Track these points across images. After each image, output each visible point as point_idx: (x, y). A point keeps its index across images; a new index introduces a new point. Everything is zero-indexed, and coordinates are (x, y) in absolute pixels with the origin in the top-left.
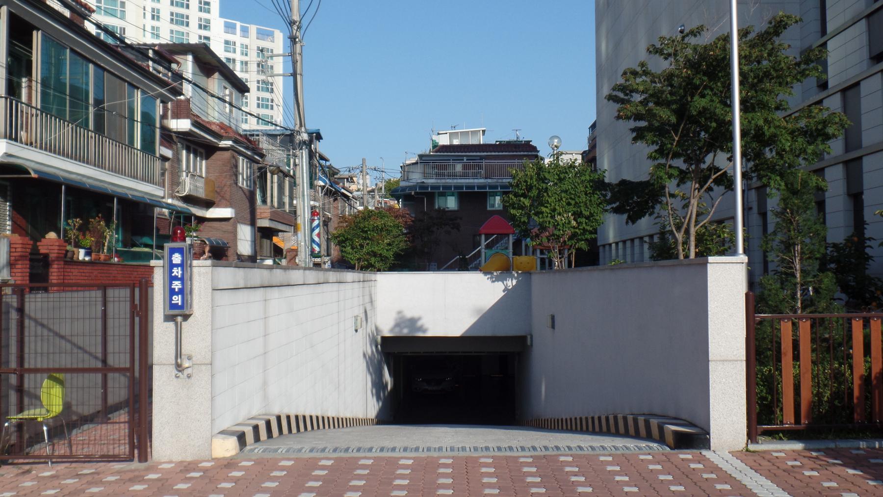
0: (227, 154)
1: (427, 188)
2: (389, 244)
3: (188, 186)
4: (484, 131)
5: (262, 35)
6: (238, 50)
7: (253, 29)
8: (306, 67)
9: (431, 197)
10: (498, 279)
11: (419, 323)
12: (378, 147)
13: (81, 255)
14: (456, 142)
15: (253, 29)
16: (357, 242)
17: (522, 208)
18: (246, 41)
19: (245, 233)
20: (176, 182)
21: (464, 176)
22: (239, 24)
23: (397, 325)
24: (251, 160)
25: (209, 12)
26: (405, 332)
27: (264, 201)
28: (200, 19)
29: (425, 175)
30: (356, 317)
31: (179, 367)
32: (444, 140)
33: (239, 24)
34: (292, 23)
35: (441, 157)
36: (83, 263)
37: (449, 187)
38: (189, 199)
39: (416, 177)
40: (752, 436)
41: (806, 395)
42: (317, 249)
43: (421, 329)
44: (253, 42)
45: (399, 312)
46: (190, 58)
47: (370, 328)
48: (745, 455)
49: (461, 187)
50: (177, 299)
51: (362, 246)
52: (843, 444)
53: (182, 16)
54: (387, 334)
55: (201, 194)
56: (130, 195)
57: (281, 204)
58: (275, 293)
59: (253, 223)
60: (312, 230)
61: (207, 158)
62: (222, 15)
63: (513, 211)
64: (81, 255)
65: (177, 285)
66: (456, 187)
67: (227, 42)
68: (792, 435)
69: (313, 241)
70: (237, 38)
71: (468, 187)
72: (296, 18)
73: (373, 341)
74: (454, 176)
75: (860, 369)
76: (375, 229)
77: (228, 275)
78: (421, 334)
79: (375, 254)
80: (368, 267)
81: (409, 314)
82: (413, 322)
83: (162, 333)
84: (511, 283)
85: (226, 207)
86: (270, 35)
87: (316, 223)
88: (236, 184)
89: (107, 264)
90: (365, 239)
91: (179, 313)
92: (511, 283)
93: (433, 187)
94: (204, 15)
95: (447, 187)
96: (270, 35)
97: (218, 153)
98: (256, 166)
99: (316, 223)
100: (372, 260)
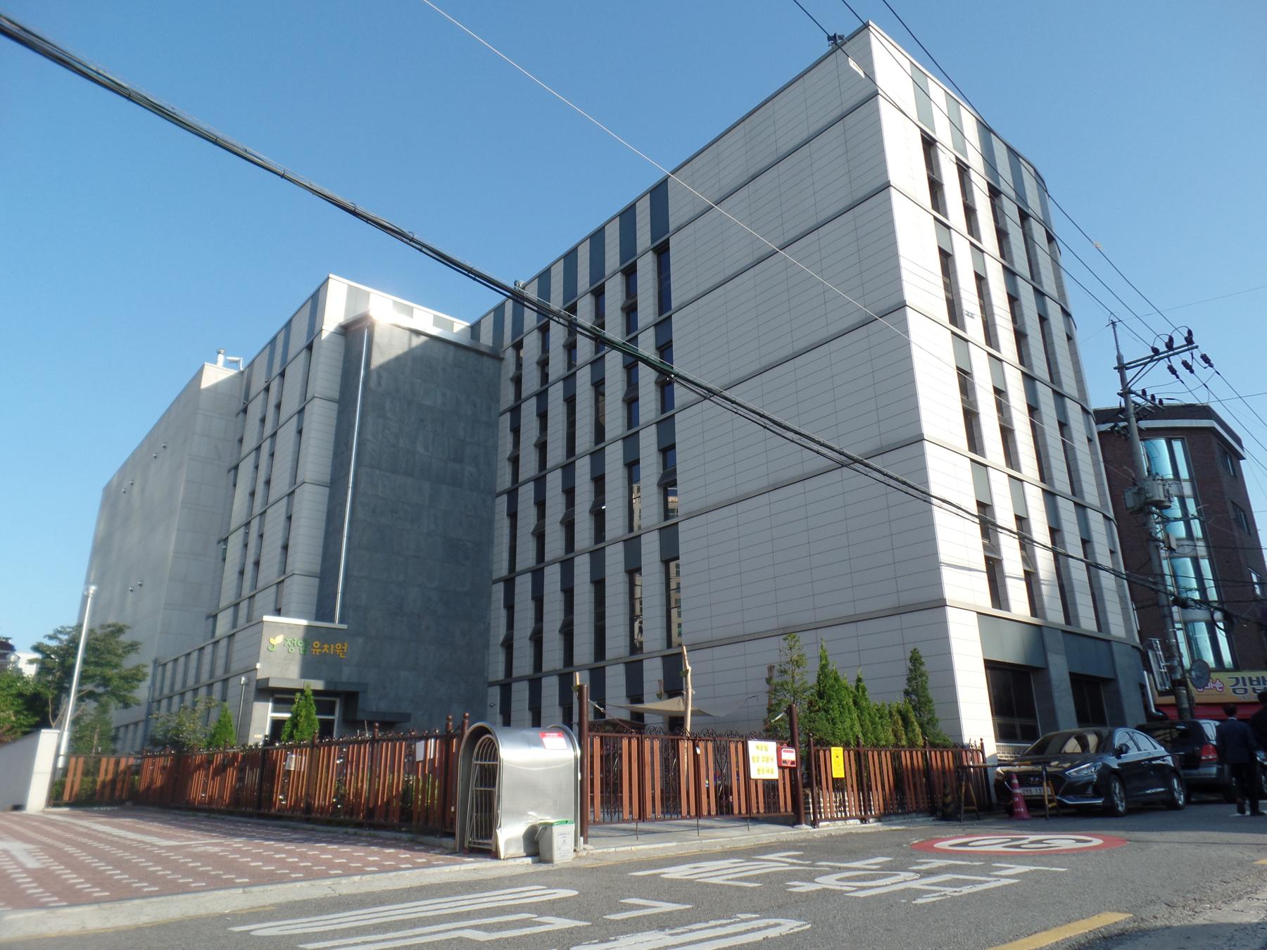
68: (66, 805)
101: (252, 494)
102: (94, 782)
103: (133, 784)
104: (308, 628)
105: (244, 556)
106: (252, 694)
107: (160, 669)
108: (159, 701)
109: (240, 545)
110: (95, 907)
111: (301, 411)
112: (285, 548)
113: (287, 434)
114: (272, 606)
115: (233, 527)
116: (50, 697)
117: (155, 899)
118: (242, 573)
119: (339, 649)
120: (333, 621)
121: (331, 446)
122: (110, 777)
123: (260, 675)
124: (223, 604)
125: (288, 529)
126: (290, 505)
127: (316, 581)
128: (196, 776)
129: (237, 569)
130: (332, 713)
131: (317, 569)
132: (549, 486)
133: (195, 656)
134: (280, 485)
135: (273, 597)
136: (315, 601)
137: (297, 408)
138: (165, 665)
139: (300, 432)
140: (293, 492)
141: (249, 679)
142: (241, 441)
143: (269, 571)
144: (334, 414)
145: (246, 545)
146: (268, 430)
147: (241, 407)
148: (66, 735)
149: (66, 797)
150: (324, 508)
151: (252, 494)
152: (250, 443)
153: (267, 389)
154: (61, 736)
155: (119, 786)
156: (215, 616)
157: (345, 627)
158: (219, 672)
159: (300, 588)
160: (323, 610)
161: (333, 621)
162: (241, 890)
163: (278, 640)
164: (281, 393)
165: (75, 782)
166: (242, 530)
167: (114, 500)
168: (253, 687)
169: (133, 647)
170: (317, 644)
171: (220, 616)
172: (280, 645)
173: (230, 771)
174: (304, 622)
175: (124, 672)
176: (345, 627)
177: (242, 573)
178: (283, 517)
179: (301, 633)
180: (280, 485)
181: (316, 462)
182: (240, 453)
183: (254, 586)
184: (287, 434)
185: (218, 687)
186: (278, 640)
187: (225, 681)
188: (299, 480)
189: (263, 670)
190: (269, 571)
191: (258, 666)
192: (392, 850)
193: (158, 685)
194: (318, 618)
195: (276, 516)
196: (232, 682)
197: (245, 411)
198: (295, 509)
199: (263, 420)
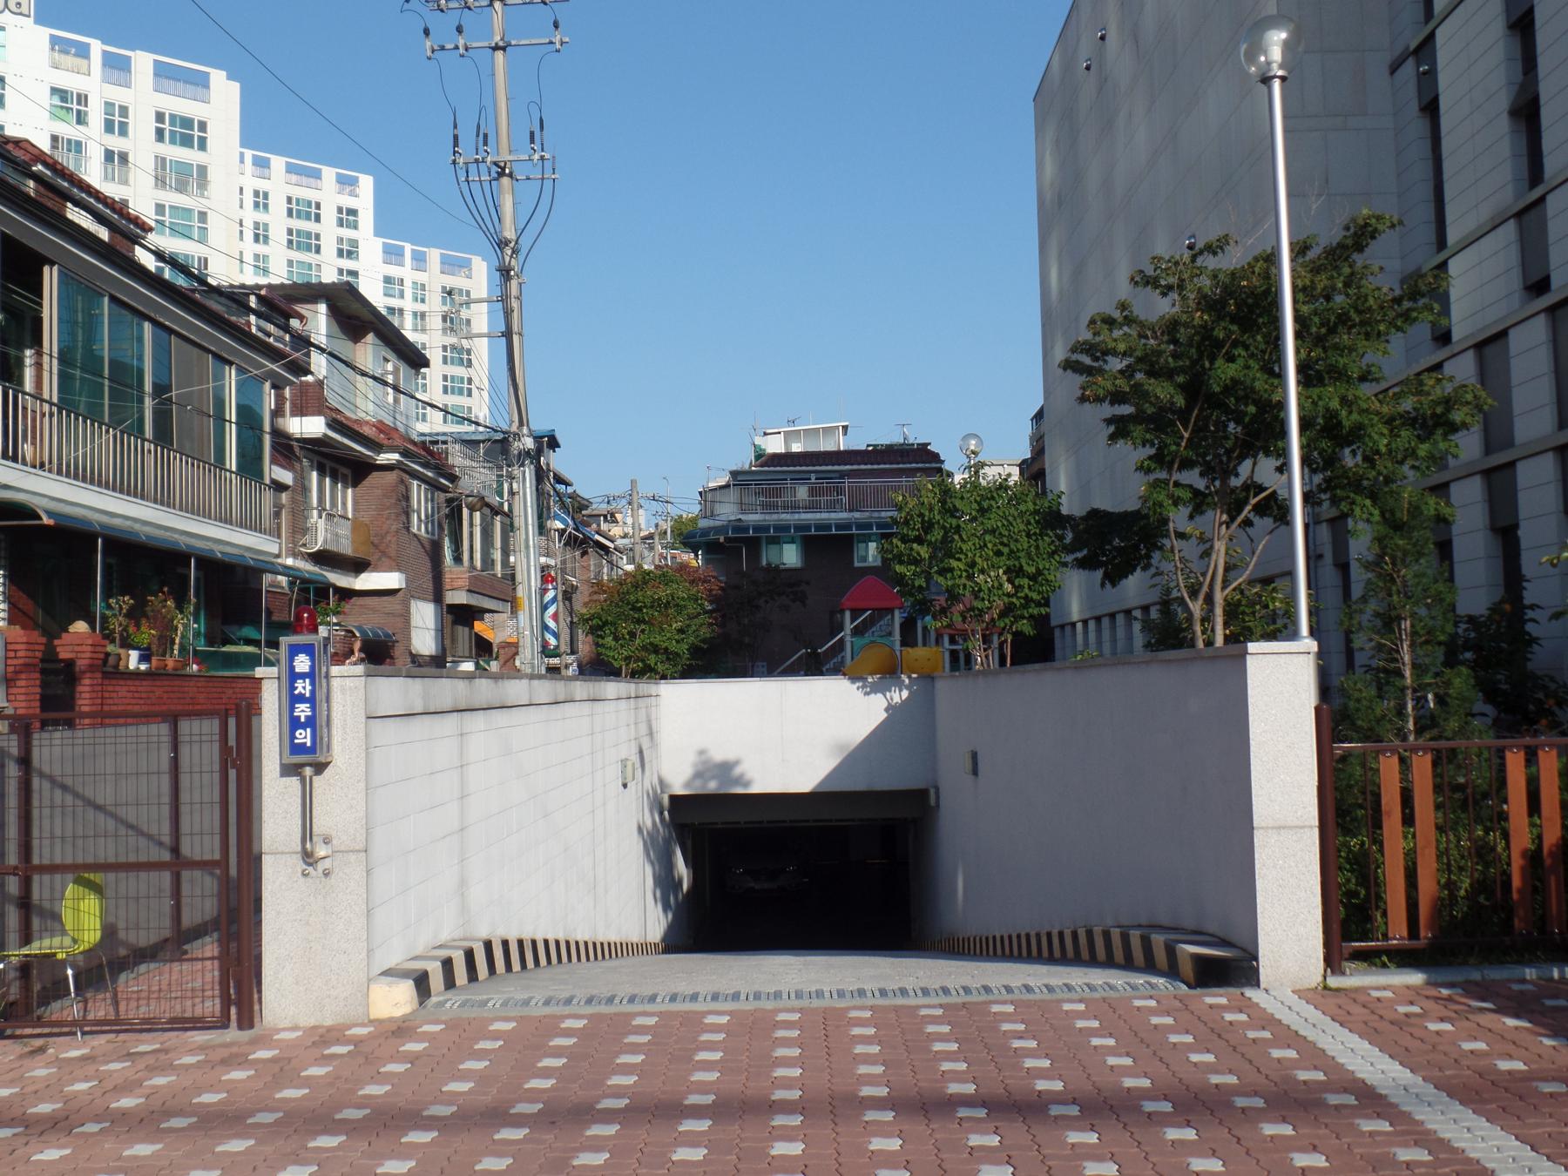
0: (391, 477)
1: (746, 529)
2: (681, 631)
3: (321, 535)
5: (449, 265)
6: (408, 293)
7: (434, 255)
8: (530, 321)
10: (875, 689)
11: (737, 771)
12: (655, 462)
14: (796, 448)
15: (434, 255)
16: (624, 628)
17: (916, 562)
18: (422, 277)
20: (300, 528)
21: (812, 507)
23: (698, 775)
24: (434, 486)
25: (356, 228)
26: (712, 786)
27: (458, 559)
28: (340, 240)
30: (624, 762)
31: (308, 857)
32: (775, 445)
33: (408, 248)
34: (502, 244)
36: (137, 674)
37: (786, 528)
38: (324, 558)
39: (727, 511)
40: (1332, 961)
41: (1428, 886)
43: (739, 780)
45: (702, 752)
47: (650, 780)
48: (1322, 996)
49: (807, 527)
50: (304, 737)
51: (632, 635)
53: (309, 235)
55: (346, 547)
56: (218, 552)
57: (488, 562)
58: (477, 721)
59: (438, 598)
60: (544, 608)
61: (355, 484)
62: (378, 233)
63: (899, 568)
64: (133, 660)
65: (303, 711)
66: (799, 528)
68: (1404, 958)
69: (545, 627)
70: (406, 272)
71: (819, 527)
72: (509, 234)
74: (794, 507)
76: (657, 604)
77: (394, 691)
79: (655, 649)
80: (644, 672)
81: (719, 755)
83: (277, 797)
84: (898, 696)
86: (465, 265)
87: (550, 595)
88: (408, 529)
89: (179, 675)
90: (639, 621)
91: (307, 761)
92: (898, 696)
93: (757, 528)
94: (347, 233)
96: (465, 265)
98: (441, 497)
99: (550, 595)
100: (652, 660)
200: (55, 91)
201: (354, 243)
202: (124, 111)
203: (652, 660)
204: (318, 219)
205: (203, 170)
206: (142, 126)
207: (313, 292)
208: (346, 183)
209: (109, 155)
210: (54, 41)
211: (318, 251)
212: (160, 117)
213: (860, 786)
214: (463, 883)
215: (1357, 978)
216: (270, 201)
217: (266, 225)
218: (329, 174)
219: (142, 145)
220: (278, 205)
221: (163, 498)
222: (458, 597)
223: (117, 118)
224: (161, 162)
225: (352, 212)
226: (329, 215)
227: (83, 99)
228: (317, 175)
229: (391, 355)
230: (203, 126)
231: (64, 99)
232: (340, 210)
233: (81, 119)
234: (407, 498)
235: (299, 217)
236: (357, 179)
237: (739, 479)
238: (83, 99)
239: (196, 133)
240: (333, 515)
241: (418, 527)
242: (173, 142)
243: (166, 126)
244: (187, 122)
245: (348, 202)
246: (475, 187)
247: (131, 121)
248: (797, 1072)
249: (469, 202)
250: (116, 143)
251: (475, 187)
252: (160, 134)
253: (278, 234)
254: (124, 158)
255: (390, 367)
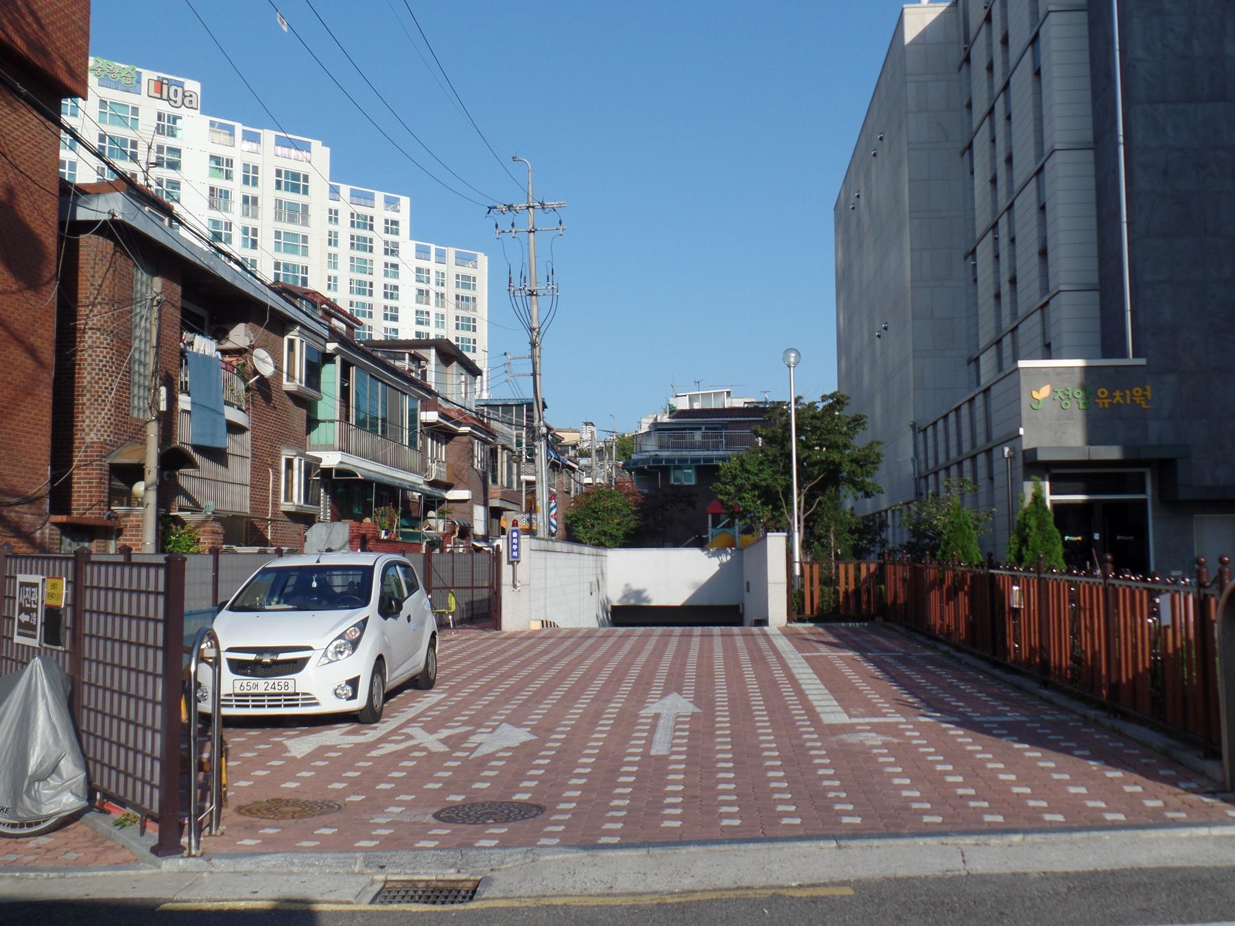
0: (465, 439)
1: (661, 461)
2: (618, 524)
3: (435, 471)
4: (728, 393)
5: (462, 260)
6: (433, 280)
7: (451, 252)
8: (543, 368)
9: (665, 471)
10: (714, 555)
11: (645, 594)
12: (609, 401)
13: (383, 536)
14: (697, 406)
15: (451, 252)
16: (589, 522)
17: (728, 494)
18: (442, 268)
19: (479, 513)
20: (424, 470)
21: (703, 446)
22: (433, 247)
23: (625, 596)
24: (484, 442)
25: (397, 234)
26: (632, 602)
27: (495, 481)
28: (386, 243)
29: (662, 447)
30: (591, 584)
31: (515, 586)
32: (683, 404)
33: (433, 247)
34: (532, 330)
35: (683, 423)
36: (384, 541)
37: (685, 460)
38: (433, 484)
39: (651, 447)
40: (790, 619)
41: (816, 601)
42: (553, 529)
43: (646, 599)
44: (451, 269)
45: (627, 585)
46: (433, 351)
47: (602, 597)
48: (786, 633)
49: (698, 460)
50: (515, 554)
51: (593, 526)
52: (834, 625)
53: (365, 239)
54: (616, 604)
55: (444, 478)
56: (386, 480)
57: (510, 482)
58: (549, 555)
59: (485, 504)
60: (550, 510)
61: (446, 443)
62: (412, 237)
63: (720, 497)
64: (383, 536)
65: (515, 547)
66: (693, 460)
67: (419, 270)
68: (811, 620)
69: (550, 523)
70: (431, 265)
71: (706, 460)
72: (535, 325)
73: (604, 609)
74: (693, 447)
75: (842, 588)
76: (606, 509)
77: (534, 543)
78: (645, 604)
79: (605, 534)
80: (600, 545)
81: (636, 586)
82: (638, 593)
83: (506, 570)
84: (726, 558)
85: (464, 489)
86: (472, 259)
87: (552, 505)
88: (472, 465)
89: (395, 542)
90: (596, 519)
91: (513, 562)
92: (726, 558)
93: (669, 460)
94: (391, 238)
95: (683, 460)
96: (472, 259)
97: (457, 438)
98: (487, 447)
99: (552, 505)
100: (603, 539)
101: (994, 181)
102: (836, 592)
103: (880, 596)
104: (1087, 369)
105: (997, 272)
106: (1020, 470)
107: (921, 435)
108: (926, 477)
109: (991, 257)
110: (643, 852)
111: (1035, 40)
112: (1043, 253)
113: (1022, 79)
114: (1038, 342)
115: (978, 234)
116: (780, 489)
117: (717, 847)
118: (998, 296)
119: (1139, 395)
120: (1124, 355)
121: (1087, 83)
122: (852, 587)
123: (1026, 445)
124: (983, 343)
125: (1043, 225)
126: (1040, 189)
127: (1095, 296)
128: (932, 593)
129: (992, 292)
130: (1143, 491)
131: (1094, 278)
132: (189, 576)
133: (952, 417)
134: (1025, 164)
135: (1038, 329)
136: (1096, 325)
137: (1028, 37)
138: (925, 430)
139: (1038, 73)
140: (1042, 168)
141: (1012, 449)
142: (969, 106)
143: (1029, 294)
144: (1084, 30)
145: (997, 257)
146: (999, 83)
147: (963, 56)
148: (797, 539)
149: (808, 611)
150: (1091, 183)
151: (994, 181)
152: (980, 108)
153: (988, 19)
154: (789, 540)
155: (864, 598)
156: (977, 360)
157: (1142, 361)
158: (981, 439)
159: (1072, 311)
160: (1111, 343)
161: (1124, 355)
162: (834, 844)
163: (1045, 392)
164: (1004, 18)
165: (815, 595)
166: (990, 235)
167: (846, 215)
168: (1020, 462)
169: (857, 421)
170: (1102, 392)
171: (983, 359)
172: (1051, 403)
173: (961, 594)
174: (1079, 363)
175: (856, 454)
176: (1142, 361)
177: (998, 296)
178: (1034, 209)
179: (1078, 378)
180: (1025, 164)
181: (1066, 112)
182: (970, 124)
183: (1014, 314)
184: (1022, 79)
185: (982, 459)
186: (1045, 392)
187: (989, 452)
188: (1047, 148)
189: (1028, 437)
190: (1029, 294)
191: (1022, 431)
192: (1118, 774)
193: (922, 456)
194: (1105, 355)
195: (1026, 204)
196: (996, 452)
197: (967, 60)
198: (1048, 193)
199: (990, 68)
200: (212, 157)
201: (396, 245)
202: (256, 169)
203: (603, 539)
204: (371, 228)
205: (305, 207)
206: (267, 179)
207: (427, 344)
208: (391, 203)
209: (245, 199)
210: (212, 124)
211: (371, 251)
212: (279, 173)
213: (705, 602)
214: (545, 606)
215: (799, 626)
216: (339, 216)
217: (336, 233)
218: (379, 196)
219: (267, 192)
220: (344, 219)
221: (397, 465)
222: (495, 503)
223: (251, 175)
224: (279, 203)
225: (395, 223)
226: (379, 225)
227: (230, 162)
228: (371, 197)
229: (464, 372)
230: (306, 178)
231: (218, 163)
232: (387, 222)
233: (228, 176)
234: (473, 450)
235: (358, 227)
236: (398, 199)
237: (657, 427)
238: (230, 162)
239: (302, 183)
240: (438, 458)
241: (477, 466)
242: (286, 189)
243: (283, 179)
244: (296, 176)
245: (392, 216)
246: (518, 299)
247: (260, 176)
248: (682, 777)
249: (515, 308)
250: (250, 191)
251: (518, 299)
252: (278, 184)
253: (344, 240)
254: (255, 200)
255: (463, 378)
